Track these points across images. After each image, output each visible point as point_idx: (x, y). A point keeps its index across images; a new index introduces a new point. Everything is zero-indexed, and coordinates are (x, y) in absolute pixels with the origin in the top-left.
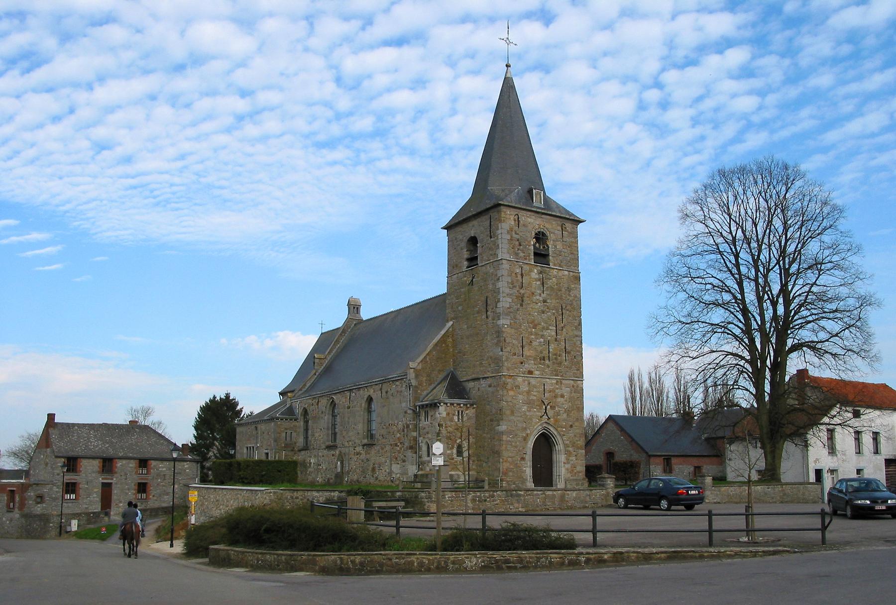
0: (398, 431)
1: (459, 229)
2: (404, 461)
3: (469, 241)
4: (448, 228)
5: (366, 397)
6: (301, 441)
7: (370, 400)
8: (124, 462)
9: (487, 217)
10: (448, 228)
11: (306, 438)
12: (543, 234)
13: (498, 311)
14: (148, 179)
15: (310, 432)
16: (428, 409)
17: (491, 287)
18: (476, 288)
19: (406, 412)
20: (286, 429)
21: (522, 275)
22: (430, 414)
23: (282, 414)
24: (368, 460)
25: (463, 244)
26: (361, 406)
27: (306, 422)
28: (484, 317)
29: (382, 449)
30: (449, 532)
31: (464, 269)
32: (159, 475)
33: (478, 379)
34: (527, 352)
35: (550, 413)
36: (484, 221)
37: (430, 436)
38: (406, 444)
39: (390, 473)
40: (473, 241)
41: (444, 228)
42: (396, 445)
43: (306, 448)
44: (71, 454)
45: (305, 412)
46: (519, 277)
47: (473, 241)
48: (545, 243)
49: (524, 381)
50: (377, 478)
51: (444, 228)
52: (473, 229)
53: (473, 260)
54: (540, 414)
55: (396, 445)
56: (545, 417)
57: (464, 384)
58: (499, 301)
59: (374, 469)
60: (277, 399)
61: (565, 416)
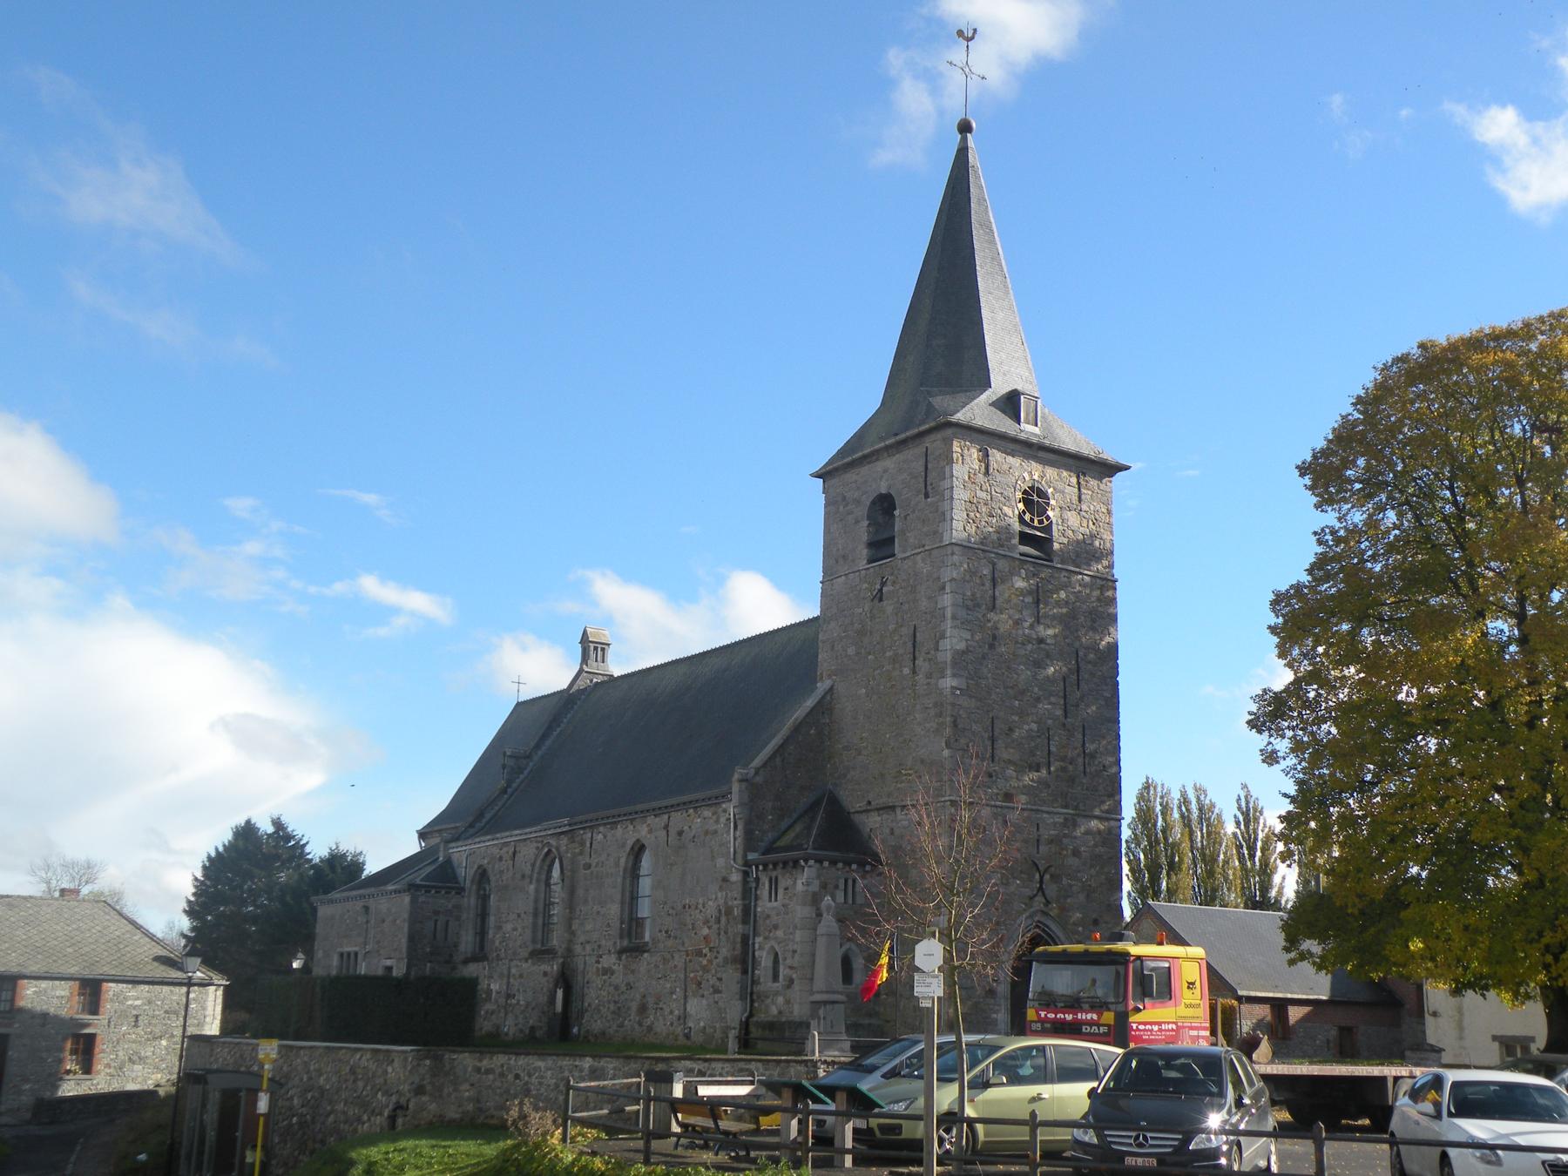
0: (706, 922)
1: (851, 476)
2: (717, 991)
3: (873, 503)
4: (824, 475)
5: (630, 843)
6: (467, 942)
7: (638, 850)
8: (44, 984)
9: (920, 450)
10: (824, 475)
11: (482, 933)
12: (1042, 494)
13: (941, 657)
14: (488, 816)
15: (492, 920)
16: (778, 872)
17: (924, 604)
18: (889, 606)
19: (725, 880)
20: (436, 913)
21: (994, 580)
22: (782, 884)
23: (427, 878)
24: (629, 986)
25: (862, 511)
26: (617, 865)
27: (484, 899)
28: (906, 671)
29: (665, 961)
30: (581, 967)
31: (863, 564)
32: (123, 1015)
33: (893, 808)
34: (1004, 754)
35: (1051, 890)
36: (913, 454)
37: (780, 933)
38: (724, 952)
39: (684, 1017)
40: (885, 505)
41: (818, 475)
42: (699, 953)
43: (475, 958)
44: (87, 974)
45: (482, 875)
46: (988, 584)
47: (885, 505)
48: (1042, 512)
49: (995, 816)
50: (650, 1029)
51: (818, 475)
52: (886, 475)
53: (881, 546)
54: (1028, 892)
55: (699, 953)
56: (1040, 898)
57: (857, 818)
58: (943, 637)
59: (643, 1009)
60: (412, 847)
61: (1082, 897)
